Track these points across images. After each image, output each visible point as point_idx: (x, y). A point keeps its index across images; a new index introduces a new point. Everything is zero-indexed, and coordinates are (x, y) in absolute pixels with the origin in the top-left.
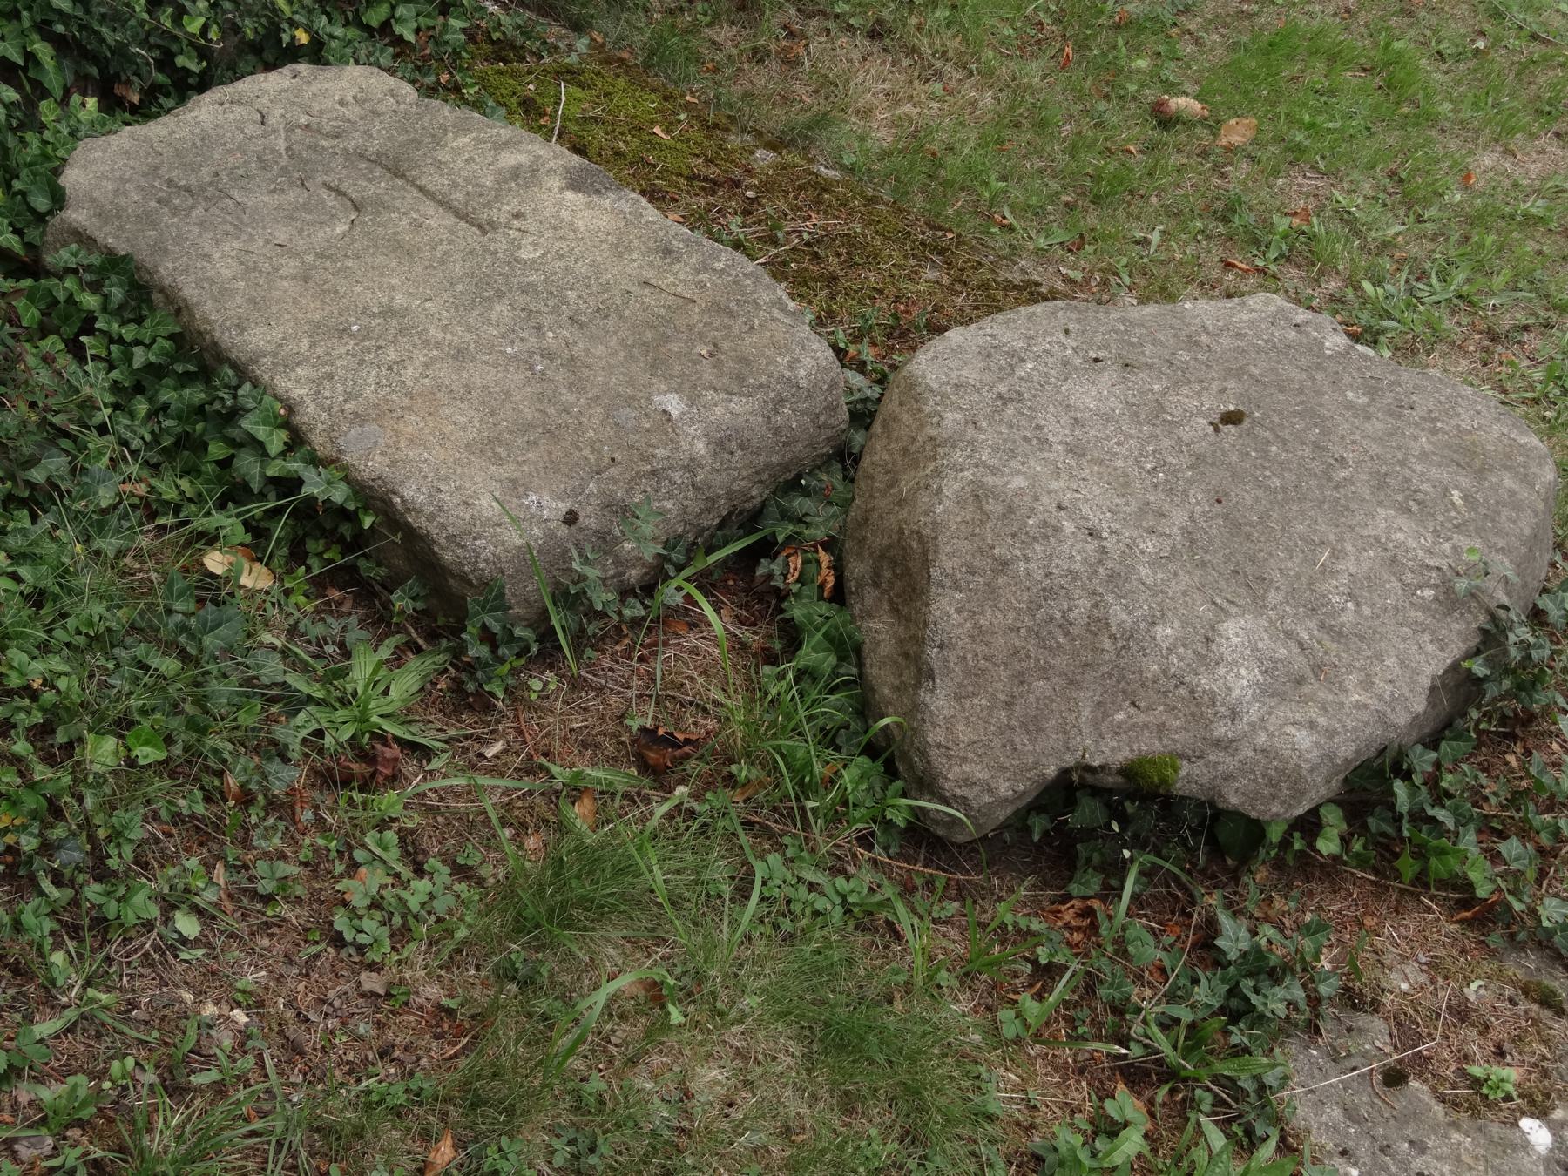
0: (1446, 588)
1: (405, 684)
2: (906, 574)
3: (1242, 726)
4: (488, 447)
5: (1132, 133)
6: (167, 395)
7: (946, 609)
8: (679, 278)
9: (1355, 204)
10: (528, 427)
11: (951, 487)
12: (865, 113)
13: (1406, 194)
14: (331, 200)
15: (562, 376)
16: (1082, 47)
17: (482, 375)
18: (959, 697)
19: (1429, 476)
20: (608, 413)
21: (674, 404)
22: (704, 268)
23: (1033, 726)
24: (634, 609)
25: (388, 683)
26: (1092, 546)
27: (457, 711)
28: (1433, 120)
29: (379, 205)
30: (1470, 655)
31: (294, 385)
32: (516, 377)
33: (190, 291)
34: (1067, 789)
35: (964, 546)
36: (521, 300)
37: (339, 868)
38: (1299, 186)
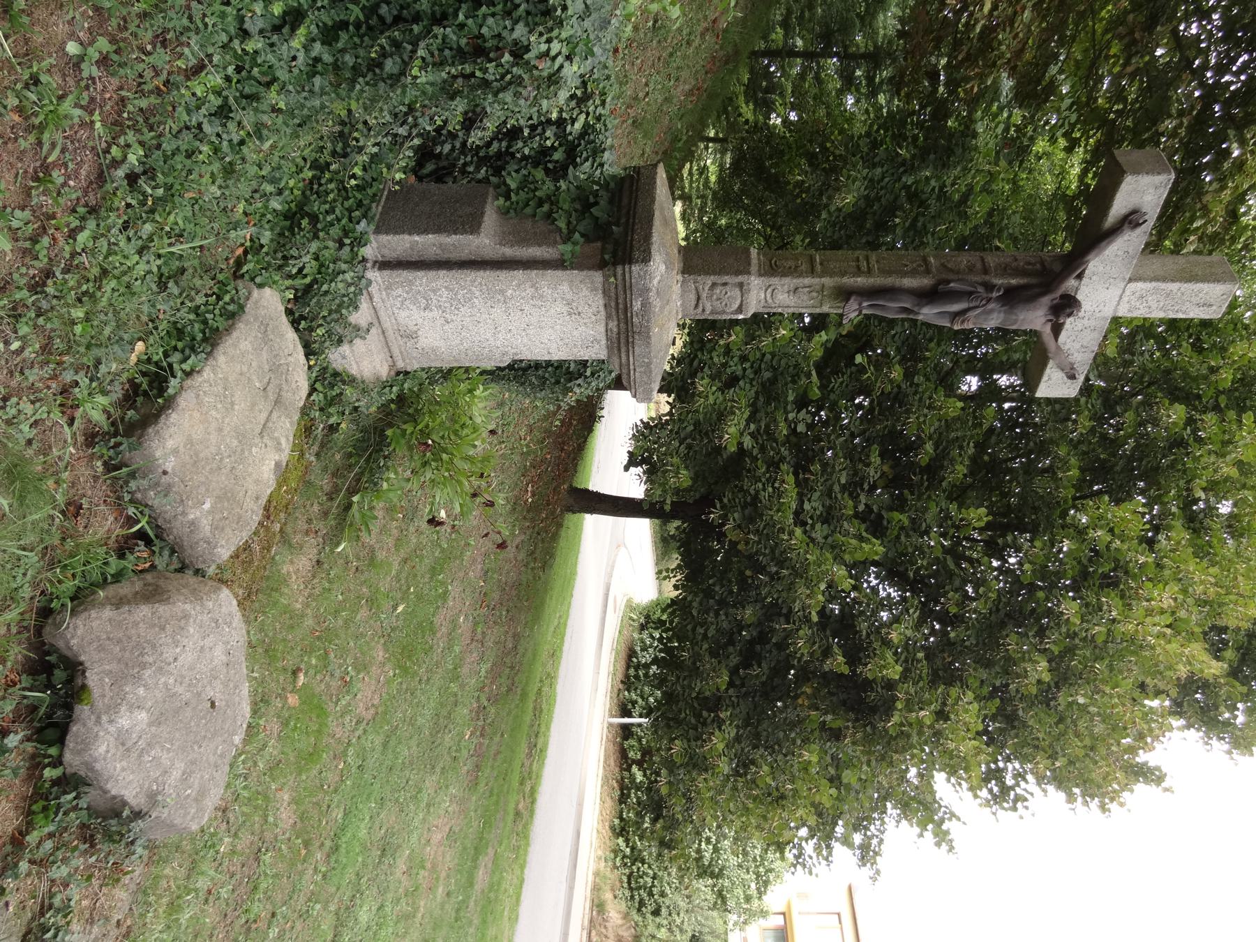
0: (158, 793)
1: (97, 416)
2: (153, 595)
3: (106, 725)
4: (190, 442)
5: (290, 662)
6: (197, 326)
7: (144, 611)
8: (249, 504)
9: (269, 749)
10: (197, 455)
11: (188, 607)
12: (292, 562)
13: (274, 768)
14: (266, 380)
15: (214, 466)
16: (319, 638)
17: (214, 438)
18: (110, 620)
19: (195, 781)
20: (203, 483)
21: (207, 506)
22: (253, 512)
23: (101, 649)
24: (127, 497)
25: (96, 410)
26: (171, 660)
27: (85, 435)
28: (300, 774)
29: (266, 397)
30: (131, 808)
31: (207, 373)
32: (213, 450)
33: (235, 334)
34: (74, 667)
35: (168, 614)
36: (239, 449)
37: (32, 398)
38: (275, 727)
